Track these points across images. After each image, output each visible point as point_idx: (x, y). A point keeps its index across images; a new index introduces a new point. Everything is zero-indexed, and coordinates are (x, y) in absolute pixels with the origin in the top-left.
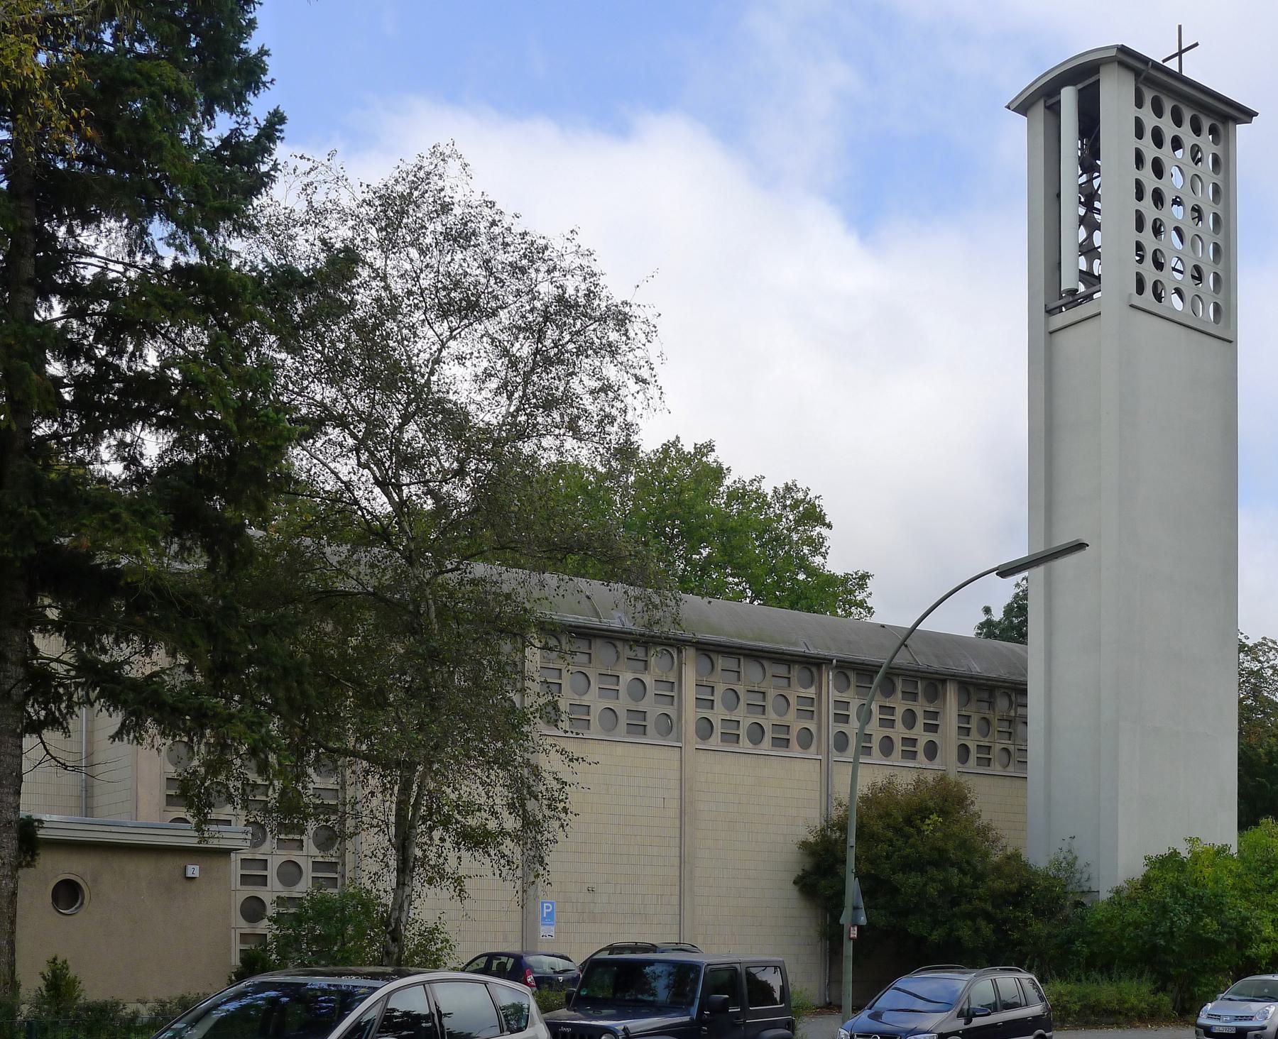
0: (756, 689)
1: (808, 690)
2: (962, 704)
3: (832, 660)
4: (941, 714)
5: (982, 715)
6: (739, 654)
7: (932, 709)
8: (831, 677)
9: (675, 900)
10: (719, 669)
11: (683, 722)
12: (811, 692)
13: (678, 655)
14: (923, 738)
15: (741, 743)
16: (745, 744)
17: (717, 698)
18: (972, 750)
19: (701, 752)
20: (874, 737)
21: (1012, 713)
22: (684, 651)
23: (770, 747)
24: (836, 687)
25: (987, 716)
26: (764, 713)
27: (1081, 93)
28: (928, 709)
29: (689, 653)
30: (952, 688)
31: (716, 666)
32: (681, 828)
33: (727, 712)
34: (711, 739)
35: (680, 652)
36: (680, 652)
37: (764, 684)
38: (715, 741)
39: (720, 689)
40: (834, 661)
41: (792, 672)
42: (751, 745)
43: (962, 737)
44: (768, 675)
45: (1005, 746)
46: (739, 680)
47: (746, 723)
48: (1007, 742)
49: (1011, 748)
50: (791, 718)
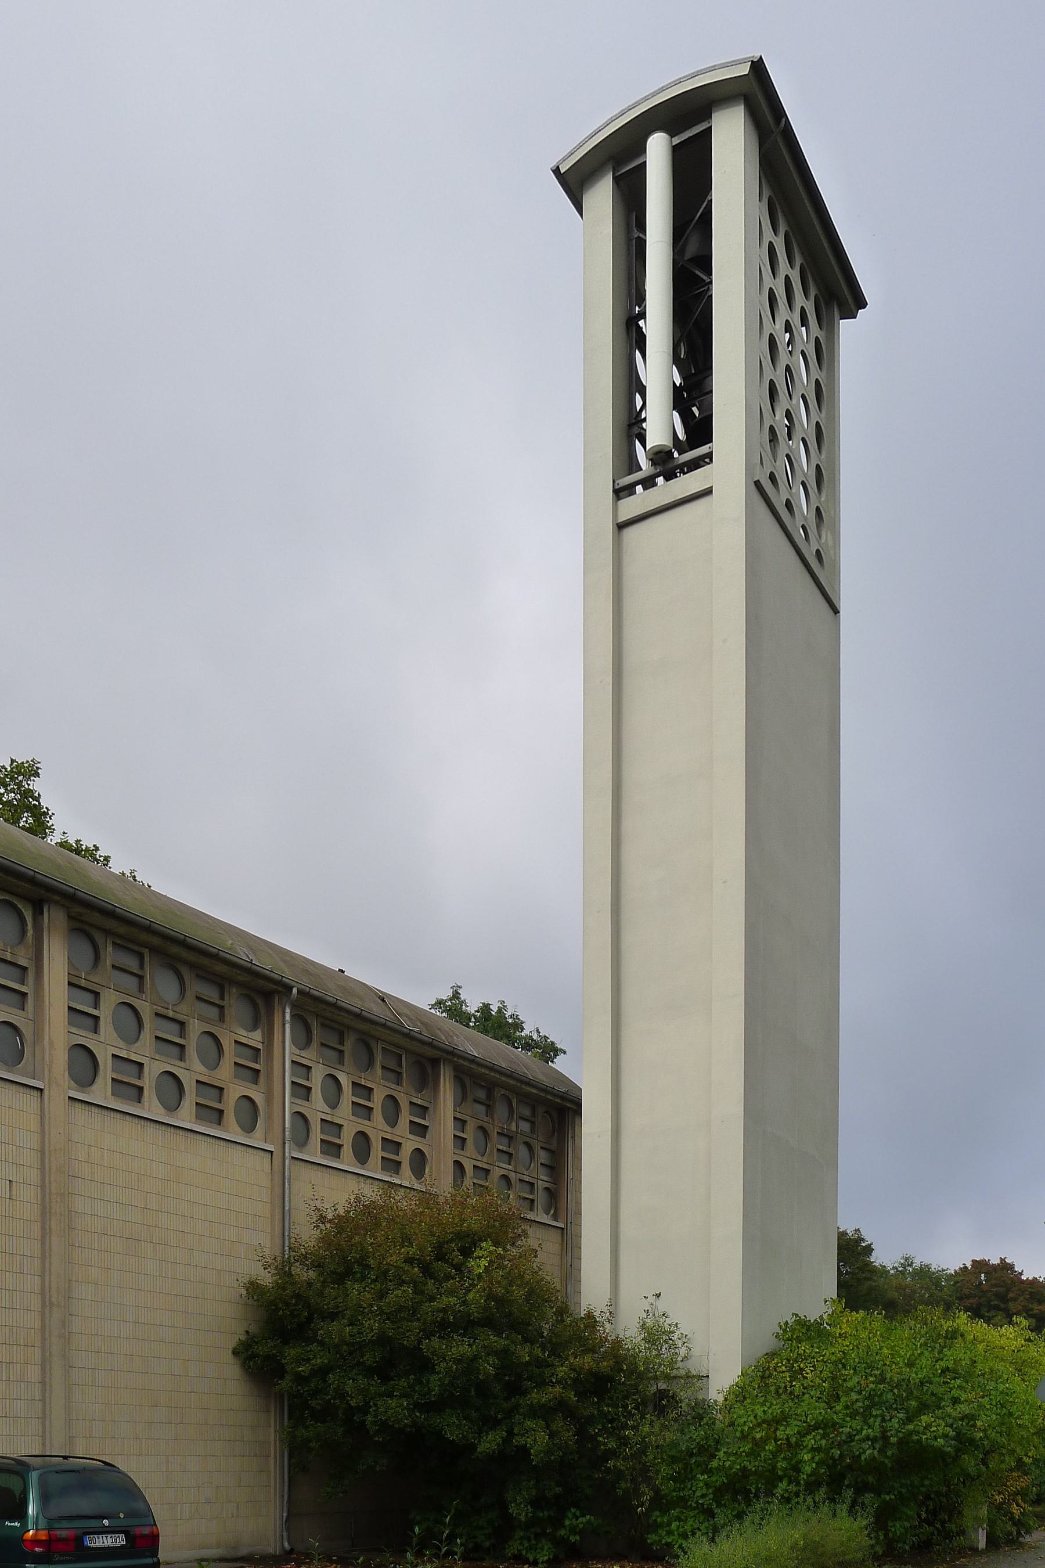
0: (171, 1014)
1: (251, 1035)
2: (457, 1105)
3: (291, 988)
4: (431, 1110)
5: (480, 1123)
6: (144, 945)
7: (419, 1102)
8: (288, 1017)
9: (34, 1373)
10: (108, 963)
11: (46, 1042)
12: (255, 1038)
13: (34, 919)
14: (410, 1144)
15: (146, 1104)
16: (152, 1107)
17: (105, 1012)
18: (467, 1174)
19: (78, 1105)
20: (345, 1128)
21: (514, 1128)
22: (45, 910)
23: (194, 1119)
24: (294, 1041)
25: (485, 1125)
26: (182, 1058)
27: (677, 152)
28: (415, 1100)
29: (54, 918)
30: (447, 1072)
31: (102, 956)
32: (43, 1436)
33: (122, 1044)
34: (94, 1087)
35: (38, 912)
36: (38, 912)
37: (183, 1008)
38: (101, 1092)
39: (110, 1000)
40: (295, 990)
41: (226, 997)
42: (162, 1110)
43: (299, 1101)
44: (190, 994)
45: (505, 1172)
46: (141, 989)
47: (154, 1069)
48: (508, 1167)
49: (512, 1176)
50: (143, 1050)
